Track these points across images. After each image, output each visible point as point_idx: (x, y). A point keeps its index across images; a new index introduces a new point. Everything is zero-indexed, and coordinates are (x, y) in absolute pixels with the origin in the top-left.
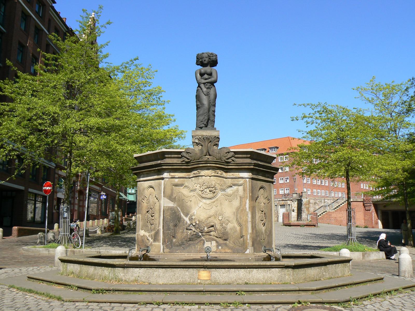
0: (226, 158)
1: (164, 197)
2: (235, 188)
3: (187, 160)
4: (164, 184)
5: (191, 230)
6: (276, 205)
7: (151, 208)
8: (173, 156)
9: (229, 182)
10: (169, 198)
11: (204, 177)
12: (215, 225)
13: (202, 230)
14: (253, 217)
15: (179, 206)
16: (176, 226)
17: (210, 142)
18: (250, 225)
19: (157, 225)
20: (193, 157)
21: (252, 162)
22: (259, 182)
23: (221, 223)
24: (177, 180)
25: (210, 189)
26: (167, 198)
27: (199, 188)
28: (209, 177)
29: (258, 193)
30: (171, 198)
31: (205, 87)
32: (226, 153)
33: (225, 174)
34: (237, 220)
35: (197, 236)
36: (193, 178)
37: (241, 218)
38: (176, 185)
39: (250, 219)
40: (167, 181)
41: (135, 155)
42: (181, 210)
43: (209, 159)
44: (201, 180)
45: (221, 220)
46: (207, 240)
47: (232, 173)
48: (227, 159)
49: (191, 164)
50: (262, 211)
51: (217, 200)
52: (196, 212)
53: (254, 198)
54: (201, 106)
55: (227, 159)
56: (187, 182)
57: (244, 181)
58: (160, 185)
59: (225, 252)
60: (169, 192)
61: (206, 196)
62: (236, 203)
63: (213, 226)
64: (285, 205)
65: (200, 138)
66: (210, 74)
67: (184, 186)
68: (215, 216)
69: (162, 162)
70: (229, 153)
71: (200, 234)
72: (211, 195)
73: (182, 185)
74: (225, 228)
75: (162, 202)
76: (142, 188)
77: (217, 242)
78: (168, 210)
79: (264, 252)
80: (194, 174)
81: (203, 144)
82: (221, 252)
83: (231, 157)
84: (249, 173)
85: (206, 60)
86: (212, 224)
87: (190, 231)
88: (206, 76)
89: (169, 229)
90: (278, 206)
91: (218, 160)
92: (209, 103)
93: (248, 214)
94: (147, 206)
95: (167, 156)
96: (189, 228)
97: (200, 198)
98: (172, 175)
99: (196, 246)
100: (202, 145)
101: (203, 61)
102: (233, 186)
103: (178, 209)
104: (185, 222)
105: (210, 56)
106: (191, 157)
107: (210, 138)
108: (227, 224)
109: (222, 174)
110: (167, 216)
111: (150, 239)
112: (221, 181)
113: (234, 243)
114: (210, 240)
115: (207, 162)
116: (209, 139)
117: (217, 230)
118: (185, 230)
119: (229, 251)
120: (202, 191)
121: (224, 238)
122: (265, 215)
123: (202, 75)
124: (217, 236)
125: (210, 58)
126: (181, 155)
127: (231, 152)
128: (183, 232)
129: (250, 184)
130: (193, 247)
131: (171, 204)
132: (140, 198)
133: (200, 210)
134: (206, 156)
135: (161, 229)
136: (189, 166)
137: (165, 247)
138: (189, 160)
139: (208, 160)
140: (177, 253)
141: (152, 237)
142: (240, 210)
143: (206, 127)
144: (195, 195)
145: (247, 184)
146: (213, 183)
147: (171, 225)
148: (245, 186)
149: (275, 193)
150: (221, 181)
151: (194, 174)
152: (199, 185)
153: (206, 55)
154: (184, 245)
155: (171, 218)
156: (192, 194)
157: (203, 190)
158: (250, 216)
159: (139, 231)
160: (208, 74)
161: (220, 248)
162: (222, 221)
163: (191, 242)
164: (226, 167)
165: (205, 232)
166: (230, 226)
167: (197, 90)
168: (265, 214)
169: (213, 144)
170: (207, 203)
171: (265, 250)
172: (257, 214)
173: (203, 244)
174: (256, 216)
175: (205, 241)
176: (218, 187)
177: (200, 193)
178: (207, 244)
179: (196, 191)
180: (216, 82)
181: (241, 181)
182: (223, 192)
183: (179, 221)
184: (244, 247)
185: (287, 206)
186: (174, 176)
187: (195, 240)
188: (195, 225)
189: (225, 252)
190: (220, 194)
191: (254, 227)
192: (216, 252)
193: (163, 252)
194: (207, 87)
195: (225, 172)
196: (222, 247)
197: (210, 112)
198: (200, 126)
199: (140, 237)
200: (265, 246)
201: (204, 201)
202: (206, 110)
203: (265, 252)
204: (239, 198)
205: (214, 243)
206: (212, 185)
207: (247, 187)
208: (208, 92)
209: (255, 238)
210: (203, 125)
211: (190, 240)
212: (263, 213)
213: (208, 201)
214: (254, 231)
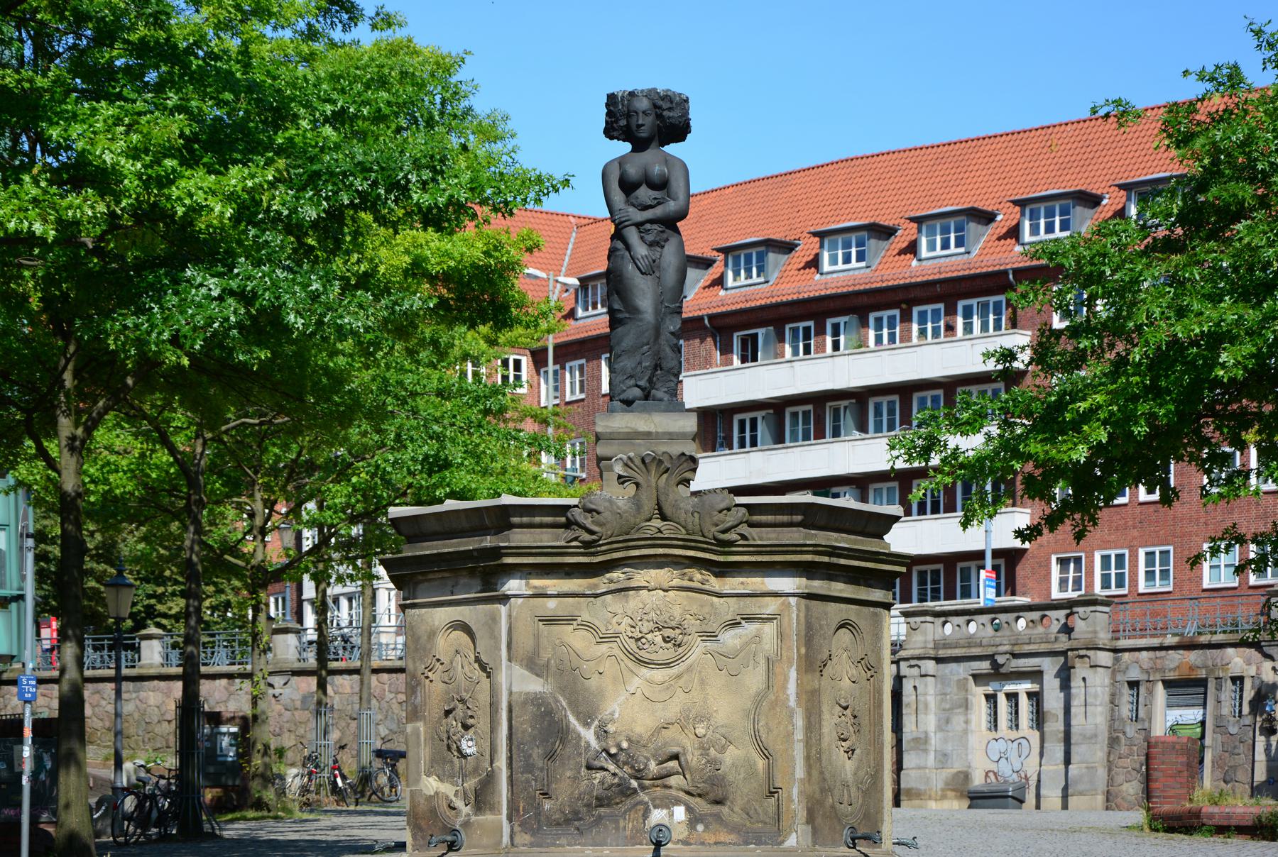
0: (721, 527)
1: (510, 660)
2: (751, 628)
4: (510, 616)
5: (603, 769)
6: (1134, 685)
7: (462, 701)
8: (537, 520)
9: (730, 608)
11: (644, 592)
13: (639, 771)
14: (812, 726)
15: (562, 690)
16: (551, 756)
17: (666, 471)
18: (799, 752)
19: (488, 757)
22: (832, 606)
23: (703, 748)
24: (552, 604)
28: (661, 593)
30: (533, 665)
31: (642, 238)
33: (715, 583)
34: (756, 737)
36: (609, 596)
37: (769, 731)
39: (799, 735)
40: (520, 606)
41: (394, 512)
42: (570, 703)
44: (634, 602)
46: (658, 802)
48: (724, 532)
49: (604, 548)
50: (845, 708)
51: (689, 669)
53: (814, 663)
55: (724, 532)
57: (783, 604)
58: (494, 619)
59: (716, 843)
61: (654, 656)
62: (754, 680)
63: (675, 757)
64: (1203, 683)
65: (630, 458)
66: (662, 185)
68: (685, 721)
71: (634, 783)
72: (667, 653)
73: (569, 620)
74: (715, 764)
75: (502, 678)
77: (689, 809)
78: (525, 703)
80: (611, 581)
81: (640, 479)
82: (703, 844)
84: (797, 580)
86: (675, 749)
87: (599, 775)
88: (644, 194)
89: (529, 768)
90: (1151, 692)
91: (694, 534)
92: (659, 303)
93: (791, 717)
94: (447, 693)
95: (516, 520)
96: (597, 763)
97: (630, 664)
99: (622, 823)
103: (557, 701)
105: (660, 108)
106: (601, 525)
107: (664, 458)
108: (723, 750)
111: (459, 803)
114: (668, 803)
115: (654, 541)
116: (660, 462)
118: (584, 771)
120: (638, 640)
121: (711, 796)
122: (856, 721)
123: (628, 187)
124: (691, 789)
125: (659, 116)
126: (567, 519)
127: (737, 505)
129: (802, 615)
130: (611, 826)
133: (633, 705)
134: (649, 520)
136: (593, 554)
137: (517, 828)
138: (594, 537)
141: (465, 797)
142: (766, 700)
143: (646, 397)
144: (617, 652)
146: (677, 612)
147: (535, 756)
148: (786, 620)
149: (1120, 584)
152: (627, 620)
153: (643, 104)
154: (580, 819)
155: (536, 732)
156: (604, 648)
158: (799, 721)
159: (418, 781)
160: (653, 186)
163: (602, 809)
164: (721, 559)
166: (731, 756)
167: (612, 253)
169: (675, 479)
171: (853, 839)
174: (824, 723)
176: (692, 624)
177: (632, 645)
178: (657, 816)
180: (683, 215)
181: (771, 606)
182: (708, 644)
185: (1219, 688)
189: (716, 843)
190: (698, 650)
191: (814, 759)
194: (650, 238)
195: (716, 575)
196: (706, 827)
197: (663, 337)
198: (623, 396)
199: (422, 801)
201: (644, 671)
204: (762, 662)
205: (680, 813)
206: (671, 617)
209: (817, 796)
210: (637, 392)
211: (601, 802)
212: (848, 712)
213: (659, 675)
214: (815, 773)
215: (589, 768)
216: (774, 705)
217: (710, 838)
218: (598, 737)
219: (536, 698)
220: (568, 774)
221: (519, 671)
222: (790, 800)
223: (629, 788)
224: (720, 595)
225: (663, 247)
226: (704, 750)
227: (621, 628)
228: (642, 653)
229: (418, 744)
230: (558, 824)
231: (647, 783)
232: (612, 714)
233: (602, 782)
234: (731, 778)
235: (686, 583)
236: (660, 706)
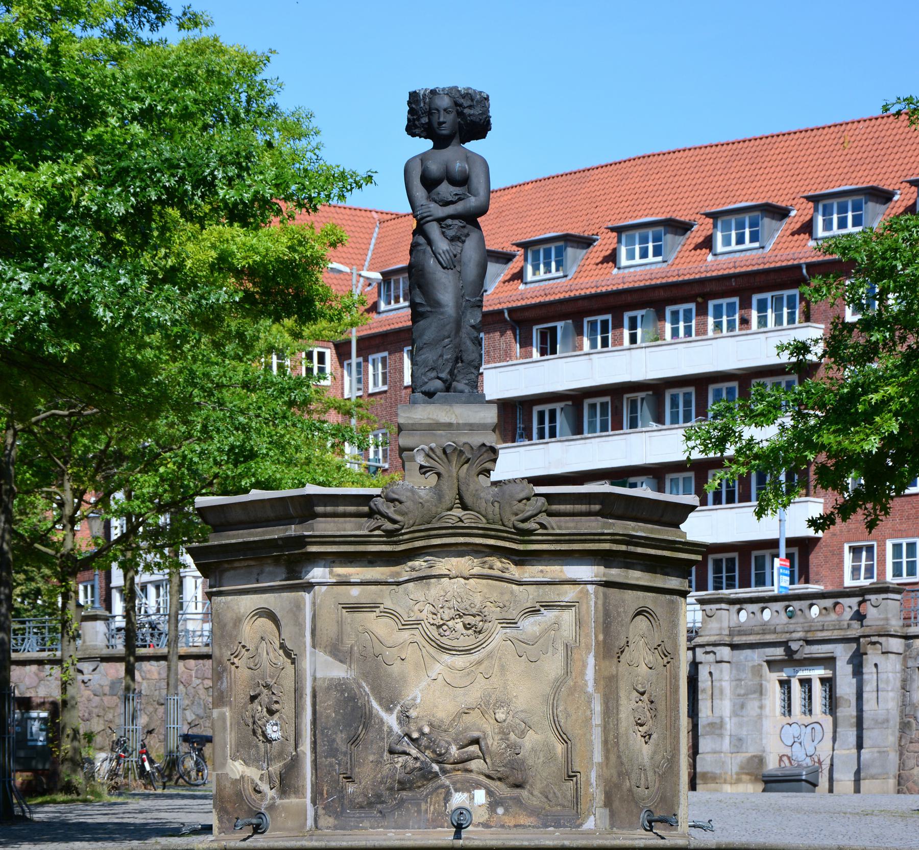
0: (521, 516)
1: (314, 646)
2: (550, 615)
3: (389, 526)
4: (314, 604)
5: (405, 753)
7: (267, 686)
8: (341, 509)
10: (330, 652)
11: (445, 580)
12: (485, 738)
13: (440, 755)
16: (354, 740)
17: (467, 462)
20: (410, 515)
21: (606, 531)
22: (629, 594)
23: (504, 733)
24: (355, 591)
25: (469, 620)
26: (325, 652)
27: (431, 616)
29: (628, 631)
30: (337, 651)
31: (443, 233)
32: (520, 501)
33: (515, 572)
34: (555, 722)
35: (427, 775)
37: (568, 715)
38: (354, 608)
39: (597, 720)
42: (373, 689)
43: (461, 521)
44: (436, 589)
45: (504, 721)
46: (459, 785)
47: (541, 568)
49: (406, 537)
50: (643, 694)
51: (490, 656)
52: (419, 695)
53: (611, 649)
54: (429, 309)
56: (388, 598)
57: (581, 592)
58: (298, 607)
59: (515, 826)
60: (328, 628)
61: (454, 643)
62: (553, 666)
63: (476, 741)
65: (431, 449)
66: (463, 181)
67: (382, 609)
68: (486, 706)
69: (306, 533)
70: (528, 499)
71: (436, 767)
72: (468, 640)
73: (372, 607)
74: (514, 748)
75: (307, 664)
76: (229, 615)
77: (489, 793)
78: (329, 688)
79: (646, 830)
81: (441, 469)
82: (503, 826)
83: (536, 515)
85: (444, 123)
86: (476, 734)
87: (402, 759)
88: (446, 190)
89: (333, 752)
91: (494, 523)
92: (460, 297)
94: (253, 679)
95: (320, 509)
96: (399, 748)
97: (432, 651)
98: (339, 575)
99: (423, 807)
100: (439, 475)
101: (436, 125)
102: (542, 609)
103: (360, 686)
104: (385, 729)
106: (403, 514)
108: (522, 735)
109: (507, 569)
110: (326, 709)
111: (264, 787)
112: (502, 594)
113: (547, 797)
114: (469, 787)
117: (490, 753)
118: (386, 755)
119: (524, 820)
120: (439, 627)
122: (653, 706)
123: (430, 183)
124: (492, 773)
125: (460, 114)
126: (370, 508)
128: (378, 762)
129: (600, 602)
131: (338, 671)
132: (224, 650)
133: (433, 692)
134: (450, 509)
135: (305, 754)
138: (396, 526)
139: (457, 525)
140: (362, 828)
142: (564, 686)
143: (448, 389)
144: (419, 638)
145: (588, 603)
147: (338, 740)
148: (584, 607)
150: (502, 594)
151: (413, 569)
153: (444, 102)
154: (383, 802)
155: (339, 717)
156: (406, 635)
157: (444, 624)
159: (224, 765)
160: (454, 182)
161: (500, 811)
162: (505, 724)
163: (404, 793)
164: (521, 547)
165: (452, 761)
166: (531, 740)
167: (414, 247)
168: (652, 702)
170: (458, 667)
172: (623, 701)
173: (445, 799)
175: (452, 791)
176: (493, 612)
177: (434, 632)
178: (458, 799)
179: (419, 626)
181: (569, 594)
182: (508, 630)
183: (366, 726)
184: (575, 810)
186: (346, 576)
187: (420, 787)
188: (417, 739)
189: (515, 826)
190: (498, 636)
191: (611, 743)
192: (486, 825)
193: (317, 827)
194: (451, 233)
196: (506, 810)
197: (464, 330)
199: (228, 785)
200: (652, 808)
201: (446, 658)
202: (448, 328)
203: (651, 830)
205: (480, 796)
206: (472, 605)
207: (588, 613)
208: (455, 256)
209: (615, 779)
210: (438, 384)
211: (403, 785)
212: (645, 697)
213: (460, 661)
214: (613, 758)
215: (391, 752)
216: (572, 691)
217: (510, 821)
218: (400, 723)
219: (340, 684)
220: (371, 758)
221: (323, 657)
222: (588, 783)
223: (431, 772)
224: (520, 583)
225: (463, 242)
226: (504, 735)
227: (423, 616)
228: (443, 640)
229: (225, 728)
230: (361, 807)
231: (448, 767)
232: (414, 699)
233: (404, 766)
234: (530, 762)
235: (487, 571)
236: (461, 691)
